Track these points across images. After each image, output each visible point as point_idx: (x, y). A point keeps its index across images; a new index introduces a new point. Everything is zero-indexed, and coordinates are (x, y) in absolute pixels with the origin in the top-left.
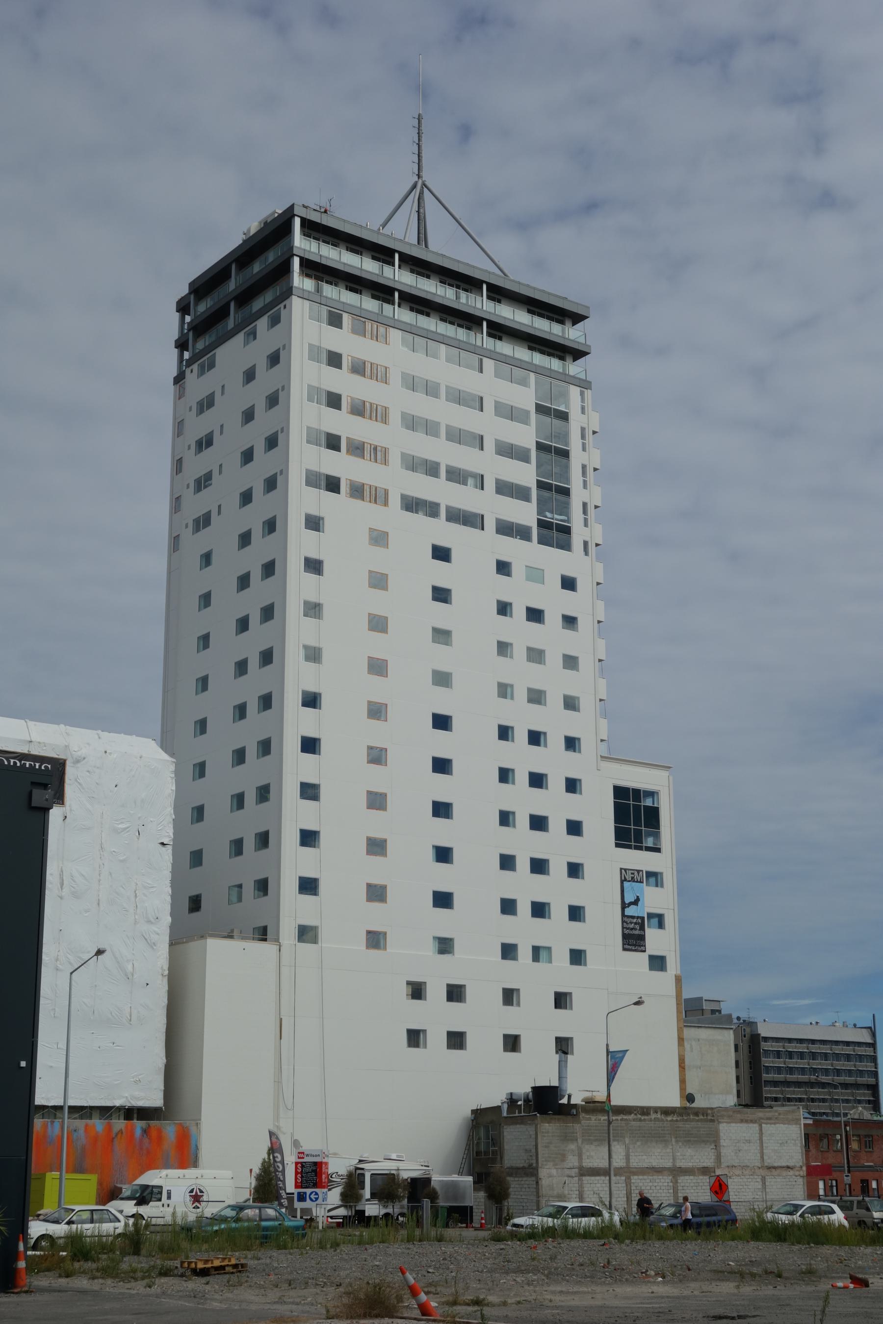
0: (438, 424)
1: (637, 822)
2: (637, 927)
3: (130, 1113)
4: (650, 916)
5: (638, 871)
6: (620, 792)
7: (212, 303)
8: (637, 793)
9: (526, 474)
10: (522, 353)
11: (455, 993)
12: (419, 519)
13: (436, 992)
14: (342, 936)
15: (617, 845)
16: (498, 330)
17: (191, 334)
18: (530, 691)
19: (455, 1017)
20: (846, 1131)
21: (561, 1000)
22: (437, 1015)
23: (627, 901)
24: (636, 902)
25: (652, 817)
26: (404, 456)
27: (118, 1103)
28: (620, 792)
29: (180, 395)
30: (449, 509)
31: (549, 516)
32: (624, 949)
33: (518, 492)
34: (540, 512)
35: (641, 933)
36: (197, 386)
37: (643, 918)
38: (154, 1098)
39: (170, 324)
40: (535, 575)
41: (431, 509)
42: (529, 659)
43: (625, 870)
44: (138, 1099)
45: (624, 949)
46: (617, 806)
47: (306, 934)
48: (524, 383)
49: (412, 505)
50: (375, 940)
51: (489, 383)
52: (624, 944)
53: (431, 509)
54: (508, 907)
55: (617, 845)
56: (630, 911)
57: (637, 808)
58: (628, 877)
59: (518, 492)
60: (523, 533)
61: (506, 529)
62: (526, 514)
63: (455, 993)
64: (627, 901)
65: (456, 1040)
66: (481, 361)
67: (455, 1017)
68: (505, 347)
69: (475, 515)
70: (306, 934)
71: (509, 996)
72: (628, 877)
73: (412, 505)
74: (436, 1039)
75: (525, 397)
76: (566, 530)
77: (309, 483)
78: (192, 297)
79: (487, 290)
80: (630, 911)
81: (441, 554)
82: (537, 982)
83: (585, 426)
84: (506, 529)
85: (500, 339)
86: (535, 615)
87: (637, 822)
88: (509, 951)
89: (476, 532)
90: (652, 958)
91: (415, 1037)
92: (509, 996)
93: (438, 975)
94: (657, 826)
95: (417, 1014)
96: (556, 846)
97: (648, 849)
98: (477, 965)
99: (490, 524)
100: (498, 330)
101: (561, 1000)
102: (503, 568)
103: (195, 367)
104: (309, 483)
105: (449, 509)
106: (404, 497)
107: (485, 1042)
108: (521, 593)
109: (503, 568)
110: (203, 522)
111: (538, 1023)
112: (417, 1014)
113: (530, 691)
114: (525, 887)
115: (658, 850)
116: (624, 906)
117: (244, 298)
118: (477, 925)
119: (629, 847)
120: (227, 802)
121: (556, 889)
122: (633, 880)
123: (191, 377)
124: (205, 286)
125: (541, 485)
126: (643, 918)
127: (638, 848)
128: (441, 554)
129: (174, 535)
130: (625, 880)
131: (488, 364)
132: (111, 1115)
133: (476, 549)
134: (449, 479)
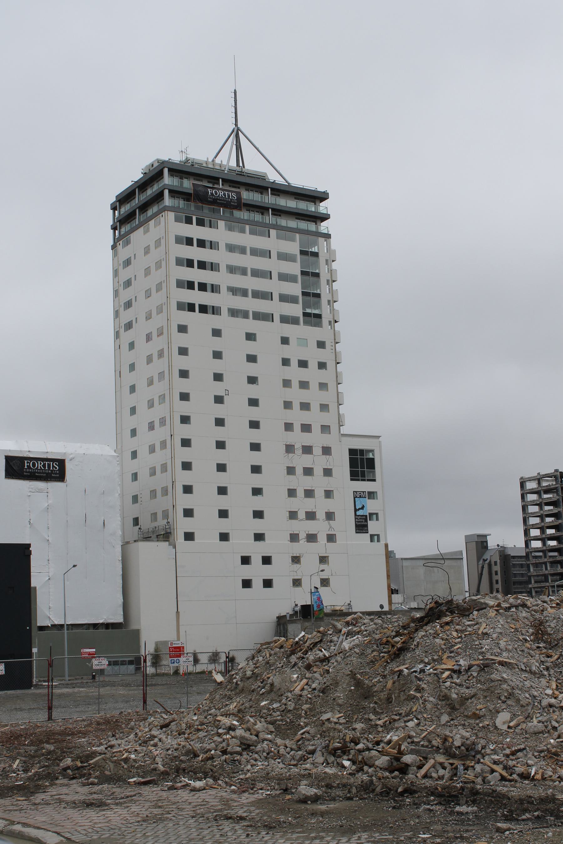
0: (246, 268)
1: (362, 467)
2: (364, 521)
3: (107, 626)
4: (371, 514)
5: (363, 492)
6: (352, 452)
7: (129, 229)
8: (362, 452)
9: (295, 289)
10: (293, 223)
11: (267, 560)
12: (239, 321)
13: (256, 560)
14: (207, 537)
15: (351, 480)
16: (278, 212)
17: (118, 223)
18: (301, 404)
19: (267, 572)
20: (472, 830)
21: (323, 560)
22: (257, 572)
23: (357, 508)
24: (363, 508)
25: (371, 464)
26: (227, 245)
27: (101, 621)
28: (352, 452)
29: (115, 255)
30: (253, 291)
31: (308, 311)
32: (356, 532)
33: (292, 300)
34: (304, 308)
35: (366, 523)
36: (124, 252)
37: (366, 516)
38: (119, 619)
39: (108, 218)
40: (303, 342)
41: (245, 314)
42: (303, 431)
43: (356, 492)
44: (111, 619)
45: (356, 532)
46: (351, 459)
47: (189, 536)
48: (293, 240)
49: (234, 313)
50: (224, 537)
51: (272, 242)
52: (356, 530)
53: (245, 314)
54: (286, 362)
55: (351, 480)
56: (359, 513)
57: (362, 460)
58: (357, 495)
59: (292, 300)
60: (294, 321)
61: (285, 319)
62: (296, 310)
63: (267, 560)
64: (357, 508)
65: (268, 583)
66: (269, 231)
67: (267, 572)
68: (283, 222)
69: (267, 293)
70: (189, 536)
71: (296, 560)
72: (357, 495)
73: (234, 313)
74: (257, 583)
75: (293, 247)
76: (319, 316)
77: (178, 286)
78: (118, 203)
79: (271, 190)
80: (359, 513)
81: (250, 337)
82: (310, 553)
83: (328, 258)
84: (285, 319)
85: (279, 195)
86: (303, 364)
87: (362, 467)
88: (294, 538)
89: (267, 259)
90: (372, 536)
91: (247, 584)
92: (296, 560)
93: (256, 551)
94: (373, 468)
95: (246, 572)
96: (318, 462)
97: (368, 480)
98: (277, 545)
99: (277, 318)
100: (278, 212)
101: (323, 560)
102: (285, 341)
103: (121, 242)
104: (178, 286)
105: (253, 291)
106: (229, 310)
107: (282, 583)
108: (294, 352)
109: (285, 341)
110: (129, 326)
111: (309, 570)
112: (246, 572)
113: (301, 404)
114: (302, 505)
115: (374, 480)
116: (356, 510)
117: (144, 207)
118: (276, 526)
119: (358, 480)
120: (148, 472)
121: (320, 505)
122: (360, 497)
123: (119, 247)
124: (125, 198)
125: (304, 294)
126: (366, 516)
127: (364, 480)
128: (250, 337)
129: (116, 331)
130: (356, 497)
131: (273, 232)
132: (98, 627)
133: (269, 333)
134: (251, 254)
